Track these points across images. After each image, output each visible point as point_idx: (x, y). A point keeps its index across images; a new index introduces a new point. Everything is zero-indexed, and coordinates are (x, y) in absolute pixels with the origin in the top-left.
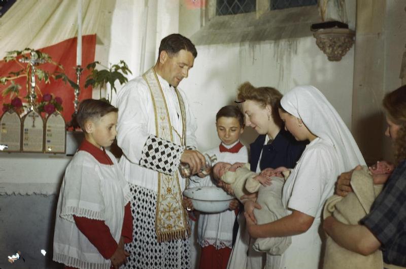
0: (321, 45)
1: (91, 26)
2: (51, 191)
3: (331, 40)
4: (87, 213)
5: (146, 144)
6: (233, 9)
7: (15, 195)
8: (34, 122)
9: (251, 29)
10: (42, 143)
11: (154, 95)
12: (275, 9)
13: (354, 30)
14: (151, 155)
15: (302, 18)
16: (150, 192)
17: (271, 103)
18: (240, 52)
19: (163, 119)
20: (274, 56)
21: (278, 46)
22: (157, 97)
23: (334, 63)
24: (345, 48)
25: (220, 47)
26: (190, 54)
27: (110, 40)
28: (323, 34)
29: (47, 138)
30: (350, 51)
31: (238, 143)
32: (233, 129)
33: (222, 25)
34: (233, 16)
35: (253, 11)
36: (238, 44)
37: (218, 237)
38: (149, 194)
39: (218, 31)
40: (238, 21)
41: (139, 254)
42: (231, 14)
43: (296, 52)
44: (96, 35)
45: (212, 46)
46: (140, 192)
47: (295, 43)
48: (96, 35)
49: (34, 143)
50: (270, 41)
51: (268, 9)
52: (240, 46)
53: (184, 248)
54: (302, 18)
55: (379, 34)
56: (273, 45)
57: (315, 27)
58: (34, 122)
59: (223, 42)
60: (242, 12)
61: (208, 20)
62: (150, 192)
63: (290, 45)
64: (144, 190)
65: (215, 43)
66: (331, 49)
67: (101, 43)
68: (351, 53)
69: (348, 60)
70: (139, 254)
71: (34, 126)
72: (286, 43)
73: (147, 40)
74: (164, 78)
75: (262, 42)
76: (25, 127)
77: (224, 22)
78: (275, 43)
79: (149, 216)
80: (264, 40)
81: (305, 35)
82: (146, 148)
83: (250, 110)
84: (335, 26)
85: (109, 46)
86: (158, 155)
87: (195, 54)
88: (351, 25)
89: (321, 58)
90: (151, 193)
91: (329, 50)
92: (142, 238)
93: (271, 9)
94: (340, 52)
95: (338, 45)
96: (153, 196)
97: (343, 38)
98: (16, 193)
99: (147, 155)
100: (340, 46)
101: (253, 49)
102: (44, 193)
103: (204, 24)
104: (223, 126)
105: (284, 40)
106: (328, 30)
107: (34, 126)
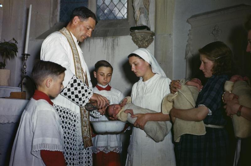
2: (13, 120)
3: (142, 37)
4: (56, 148)
5: (72, 78)
11: (71, 45)
14: (75, 86)
16: (69, 111)
19: (78, 62)
20: (103, 47)
21: (106, 41)
22: (73, 47)
24: (149, 42)
31: (108, 86)
32: (109, 75)
37: (109, 145)
38: (69, 113)
47: (117, 39)
53: (88, 151)
55: (170, 34)
56: (102, 40)
57: (133, 29)
62: (69, 111)
64: (61, 108)
72: (111, 39)
74: (74, 35)
75: (95, 38)
78: (104, 38)
79: (69, 128)
80: (96, 37)
82: (73, 80)
84: (145, 29)
86: (79, 88)
88: (152, 29)
90: (70, 112)
94: (147, 44)
95: (146, 40)
96: (71, 114)
97: (149, 36)
99: (72, 85)
100: (147, 41)
101: (89, 42)
104: (102, 72)
106: (141, 31)
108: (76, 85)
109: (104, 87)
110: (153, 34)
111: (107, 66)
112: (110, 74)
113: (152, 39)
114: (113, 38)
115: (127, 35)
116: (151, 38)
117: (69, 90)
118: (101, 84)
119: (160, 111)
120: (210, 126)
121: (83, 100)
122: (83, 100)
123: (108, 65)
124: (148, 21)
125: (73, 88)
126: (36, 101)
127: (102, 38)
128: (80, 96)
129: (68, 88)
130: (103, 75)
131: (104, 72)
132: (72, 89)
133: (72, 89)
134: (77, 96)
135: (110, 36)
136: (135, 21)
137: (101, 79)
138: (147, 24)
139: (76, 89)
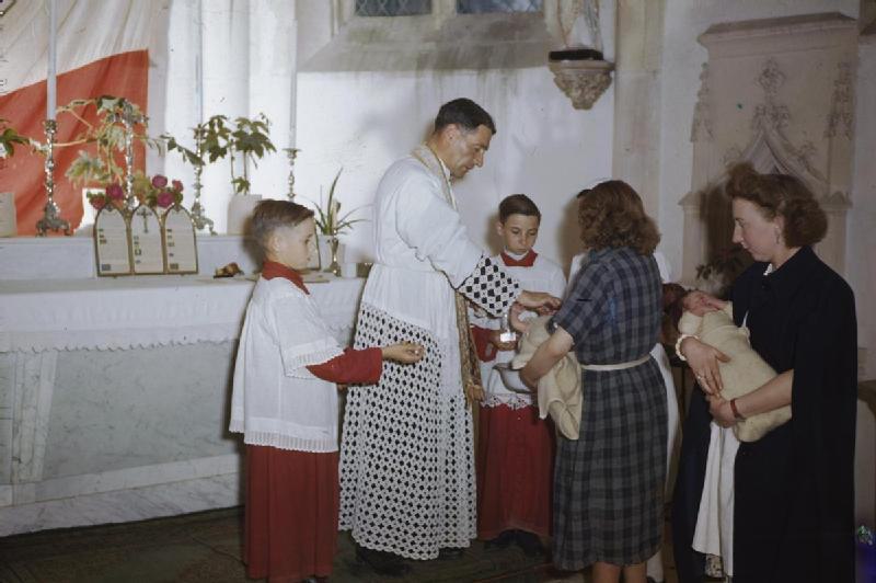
0: (565, 85)
1: (138, 34)
3: (581, 79)
6: (387, 6)
7: (173, 345)
8: (145, 224)
9: (430, 46)
10: (162, 259)
12: (465, 12)
13: (612, 61)
15: (517, 33)
17: (785, 213)
18: (417, 87)
21: (484, 80)
23: (583, 111)
25: (378, 77)
26: (490, 131)
27: (167, 59)
28: (568, 68)
29: (169, 250)
30: (607, 91)
33: (373, 36)
34: (390, 19)
35: (427, 13)
36: (413, 73)
39: (366, 46)
40: (398, 28)
41: (414, 426)
42: (384, 15)
43: (515, 92)
44: (147, 51)
45: (363, 73)
46: (404, 331)
48: (147, 51)
49: (151, 260)
50: (471, 72)
51: (453, 12)
52: (417, 76)
54: (517, 33)
56: (475, 77)
57: (556, 56)
58: (145, 224)
59: (383, 68)
60: (405, 14)
61: (342, 24)
63: (505, 79)
65: (367, 69)
66: (580, 92)
67: (155, 66)
68: (608, 97)
69: (605, 104)
70: (414, 426)
71: (146, 231)
73: (127, 27)
75: (456, 72)
76: (134, 234)
77: (373, 31)
78: (479, 74)
81: (532, 64)
83: (743, 217)
85: (166, 69)
87: (494, 132)
88: (608, 54)
89: (560, 103)
91: (576, 94)
92: (419, 402)
93: (458, 12)
95: (591, 85)
98: (156, 344)
99: (483, 271)
100: (594, 88)
102: (213, 340)
103: (336, 32)
105: (494, 71)
107: (146, 231)
108: (489, 270)
109: (518, 258)
110: (613, 67)
111: (527, 213)
112: (533, 232)
113: (608, 82)
114: (503, 72)
115: (544, 64)
116: (604, 78)
117: (477, 281)
118: (512, 251)
119: (195, 269)
120: (55, 145)
121: (503, 300)
122: (503, 300)
123: (530, 208)
124: (595, 36)
125: (486, 277)
126: (267, 282)
127: (475, 72)
128: (498, 291)
129: (475, 276)
130: (517, 232)
131: (519, 226)
132: (484, 279)
133: (484, 279)
134: (491, 293)
135: (496, 68)
136: (563, 31)
137: (514, 240)
138: (595, 40)
139: (490, 278)
